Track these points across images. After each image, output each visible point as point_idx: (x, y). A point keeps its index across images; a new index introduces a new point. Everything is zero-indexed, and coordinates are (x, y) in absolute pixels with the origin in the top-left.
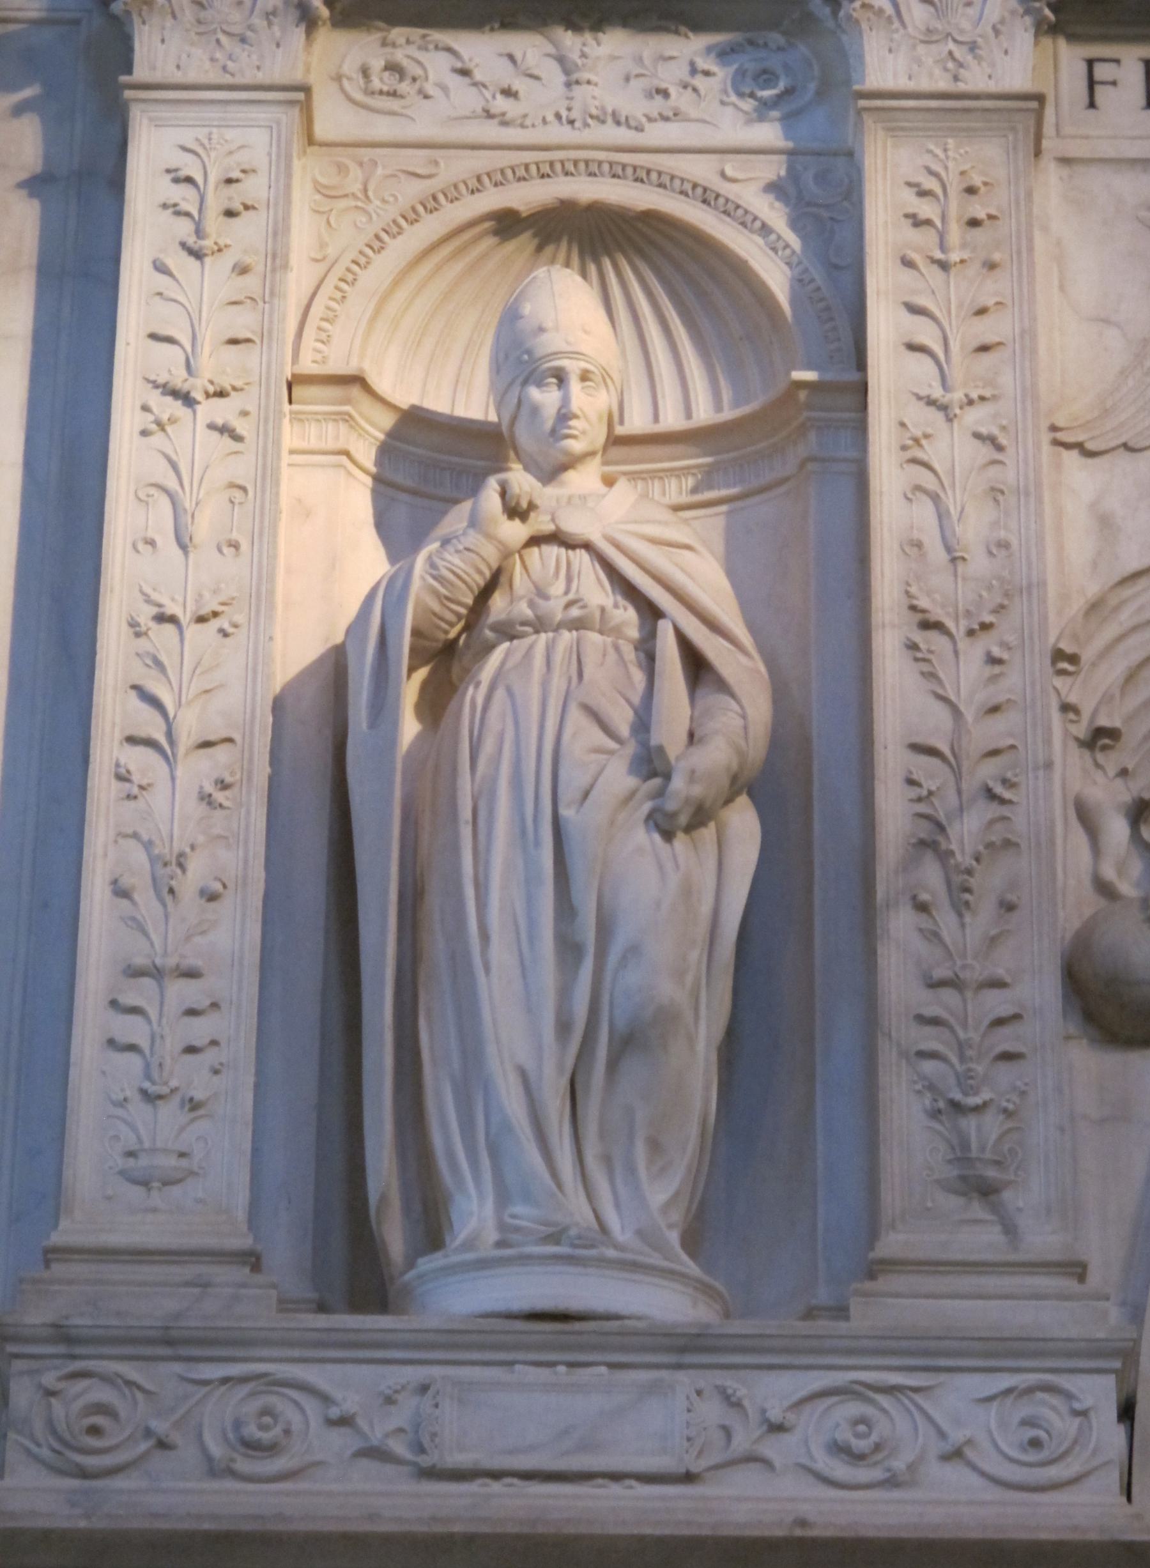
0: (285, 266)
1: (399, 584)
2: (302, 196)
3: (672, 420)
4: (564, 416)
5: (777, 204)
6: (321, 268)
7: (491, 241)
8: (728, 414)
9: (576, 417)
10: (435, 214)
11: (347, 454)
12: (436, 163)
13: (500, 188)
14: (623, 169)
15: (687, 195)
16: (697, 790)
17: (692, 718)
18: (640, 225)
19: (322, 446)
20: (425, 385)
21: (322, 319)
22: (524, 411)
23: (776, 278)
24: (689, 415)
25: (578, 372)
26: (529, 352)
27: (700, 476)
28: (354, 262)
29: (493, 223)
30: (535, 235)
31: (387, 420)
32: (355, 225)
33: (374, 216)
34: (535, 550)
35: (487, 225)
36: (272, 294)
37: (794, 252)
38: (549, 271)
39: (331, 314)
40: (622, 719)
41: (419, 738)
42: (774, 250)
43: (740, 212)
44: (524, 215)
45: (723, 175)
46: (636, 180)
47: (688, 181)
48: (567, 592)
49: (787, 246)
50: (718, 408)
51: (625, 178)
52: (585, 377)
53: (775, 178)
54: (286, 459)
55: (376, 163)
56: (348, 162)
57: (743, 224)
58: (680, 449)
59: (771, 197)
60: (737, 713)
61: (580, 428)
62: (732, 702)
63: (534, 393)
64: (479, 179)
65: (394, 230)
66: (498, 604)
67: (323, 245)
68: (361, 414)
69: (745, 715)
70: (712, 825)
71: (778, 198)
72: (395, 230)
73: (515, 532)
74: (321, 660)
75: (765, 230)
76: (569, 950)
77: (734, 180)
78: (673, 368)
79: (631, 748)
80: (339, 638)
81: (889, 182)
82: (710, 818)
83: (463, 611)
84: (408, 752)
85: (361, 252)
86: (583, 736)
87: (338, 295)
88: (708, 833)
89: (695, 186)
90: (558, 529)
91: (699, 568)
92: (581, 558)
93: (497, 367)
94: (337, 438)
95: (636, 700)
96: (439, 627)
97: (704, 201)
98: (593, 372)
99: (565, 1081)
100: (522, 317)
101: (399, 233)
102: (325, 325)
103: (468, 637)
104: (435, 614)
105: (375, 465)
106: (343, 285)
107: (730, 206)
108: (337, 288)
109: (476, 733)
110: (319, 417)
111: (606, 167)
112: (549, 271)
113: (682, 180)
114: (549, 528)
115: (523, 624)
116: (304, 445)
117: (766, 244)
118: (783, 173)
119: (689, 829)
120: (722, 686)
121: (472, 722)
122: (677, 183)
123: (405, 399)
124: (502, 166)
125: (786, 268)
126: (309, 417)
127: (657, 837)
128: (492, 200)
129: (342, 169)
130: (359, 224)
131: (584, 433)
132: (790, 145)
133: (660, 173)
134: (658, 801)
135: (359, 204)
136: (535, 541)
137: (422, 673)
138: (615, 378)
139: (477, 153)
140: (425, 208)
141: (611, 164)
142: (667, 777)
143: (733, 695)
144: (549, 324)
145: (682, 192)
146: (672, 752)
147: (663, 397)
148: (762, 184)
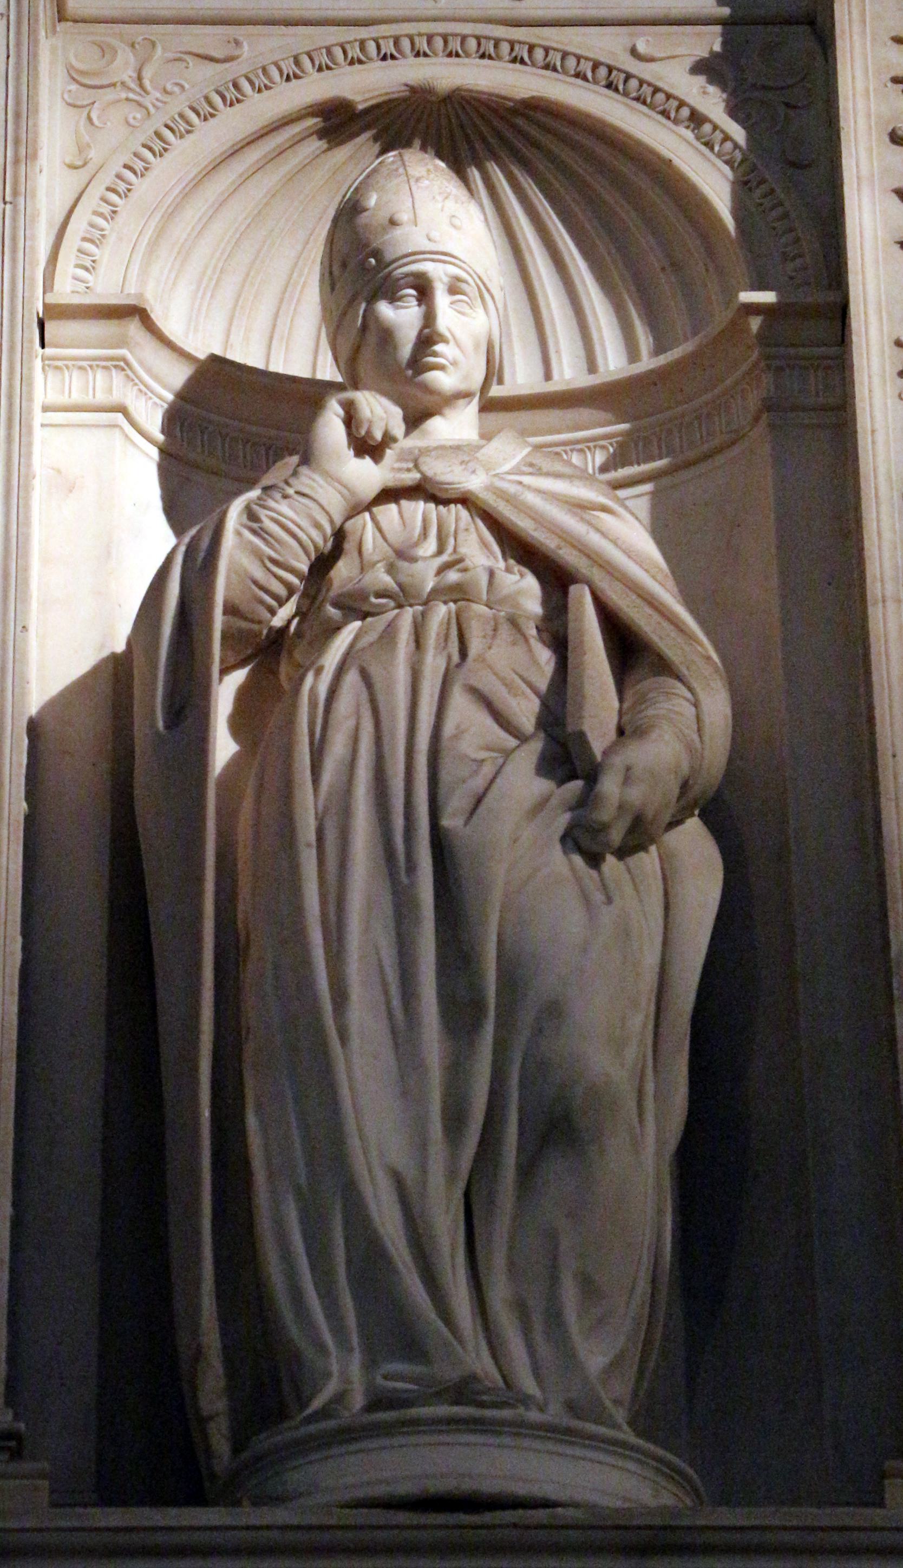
0: (32, 156)
1: (205, 543)
2: (51, 88)
3: (569, 373)
4: (427, 339)
5: (712, 89)
6: (84, 175)
7: (316, 145)
8: (647, 363)
9: (445, 341)
10: (238, 106)
11: (122, 409)
12: (237, 43)
13: (326, 73)
14: (496, 46)
15: (585, 78)
16: (636, 795)
17: (621, 713)
18: (520, 121)
19: (88, 399)
20: (228, 336)
21: (84, 239)
22: (372, 339)
23: (715, 185)
24: (592, 367)
25: (446, 279)
26: (377, 254)
27: (611, 450)
28: (126, 166)
29: (318, 119)
30: (376, 139)
31: (179, 375)
32: (128, 123)
33: (152, 110)
34: (393, 507)
35: (311, 122)
36: (15, 193)
37: (736, 146)
38: (400, 155)
39: (97, 234)
40: (526, 711)
41: (235, 763)
42: (709, 145)
43: (660, 97)
44: (360, 107)
45: (634, 52)
46: (514, 61)
47: (587, 59)
48: (440, 551)
49: (727, 138)
50: (633, 354)
51: (499, 58)
52: (453, 290)
53: (706, 54)
54: (39, 417)
55: (153, 44)
56: (115, 42)
57: (665, 113)
58: (585, 414)
59: (701, 80)
60: (688, 700)
61: (450, 358)
62: (679, 685)
63: (385, 309)
64: (297, 62)
65: (180, 127)
66: (343, 571)
67: (82, 148)
68: (141, 363)
69: (692, 725)
70: (653, 848)
71: (711, 81)
72: (183, 126)
73: (368, 475)
74: (95, 671)
75: (697, 119)
76: (461, 1014)
77: (651, 60)
78: (570, 312)
79: (536, 746)
80: (120, 646)
81: (869, 38)
82: (652, 841)
83: (295, 581)
84: (221, 775)
85: (136, 155)
86: (468, 723)
87: (106, 209)
88: (649, 860)
89: (596, 65)
90: (425, 478)
91: (624, 538)
92: (458, 515)
93: (330, 281)
94: (110, 390)
95: (543, 685)
96: (262, 602)
97: (609, 86)
98: (466, 282)
99: (459, 1193)
100: (365, 210)
101: (188, 132)
102: (88, 246)
103: (299, 624)
104: (256, 583)
105: (163, 432)
106: (113, 197)
107: (647, 90)
108: (104, 200)
109: (318, 735)
110: (84, 364)
111: (472, 43)
112: (400, 155)
113: (579, 58)
114: (411, 477)
115: (379, 595)
116: (64, 400)
117: (698, 138)
118: (717, 48)
119: (622, 853)
120: (663, 667)
121: (312, 724)
122: (571, 63)
123: (203, 345)
124: (327, 44)
125: (726, 169)
126: (70, 363)
127: (578, 860)
128: (316, 88)
129: (105, 50)
130: (132, 121)
131: (454, 363)
132: (726, 11)
133: (547, 50)
134: (580, 811)
135: (131, 96)
136: (389, 495)
137: (239, 677)
138: (496, 297)
139: (292, 30)
140: (223, 98)
141: (478, 38)
142: (592, 775)
143: (679, 678)
144: (404, 217)
145: (577, 75)
146: (598, 746)
147: (558, 352)
148: (688, 62)
